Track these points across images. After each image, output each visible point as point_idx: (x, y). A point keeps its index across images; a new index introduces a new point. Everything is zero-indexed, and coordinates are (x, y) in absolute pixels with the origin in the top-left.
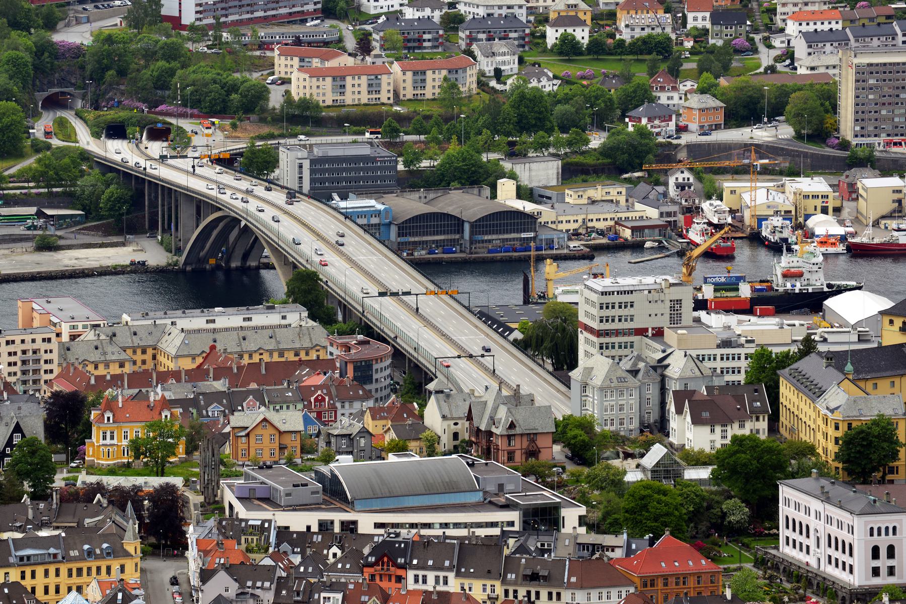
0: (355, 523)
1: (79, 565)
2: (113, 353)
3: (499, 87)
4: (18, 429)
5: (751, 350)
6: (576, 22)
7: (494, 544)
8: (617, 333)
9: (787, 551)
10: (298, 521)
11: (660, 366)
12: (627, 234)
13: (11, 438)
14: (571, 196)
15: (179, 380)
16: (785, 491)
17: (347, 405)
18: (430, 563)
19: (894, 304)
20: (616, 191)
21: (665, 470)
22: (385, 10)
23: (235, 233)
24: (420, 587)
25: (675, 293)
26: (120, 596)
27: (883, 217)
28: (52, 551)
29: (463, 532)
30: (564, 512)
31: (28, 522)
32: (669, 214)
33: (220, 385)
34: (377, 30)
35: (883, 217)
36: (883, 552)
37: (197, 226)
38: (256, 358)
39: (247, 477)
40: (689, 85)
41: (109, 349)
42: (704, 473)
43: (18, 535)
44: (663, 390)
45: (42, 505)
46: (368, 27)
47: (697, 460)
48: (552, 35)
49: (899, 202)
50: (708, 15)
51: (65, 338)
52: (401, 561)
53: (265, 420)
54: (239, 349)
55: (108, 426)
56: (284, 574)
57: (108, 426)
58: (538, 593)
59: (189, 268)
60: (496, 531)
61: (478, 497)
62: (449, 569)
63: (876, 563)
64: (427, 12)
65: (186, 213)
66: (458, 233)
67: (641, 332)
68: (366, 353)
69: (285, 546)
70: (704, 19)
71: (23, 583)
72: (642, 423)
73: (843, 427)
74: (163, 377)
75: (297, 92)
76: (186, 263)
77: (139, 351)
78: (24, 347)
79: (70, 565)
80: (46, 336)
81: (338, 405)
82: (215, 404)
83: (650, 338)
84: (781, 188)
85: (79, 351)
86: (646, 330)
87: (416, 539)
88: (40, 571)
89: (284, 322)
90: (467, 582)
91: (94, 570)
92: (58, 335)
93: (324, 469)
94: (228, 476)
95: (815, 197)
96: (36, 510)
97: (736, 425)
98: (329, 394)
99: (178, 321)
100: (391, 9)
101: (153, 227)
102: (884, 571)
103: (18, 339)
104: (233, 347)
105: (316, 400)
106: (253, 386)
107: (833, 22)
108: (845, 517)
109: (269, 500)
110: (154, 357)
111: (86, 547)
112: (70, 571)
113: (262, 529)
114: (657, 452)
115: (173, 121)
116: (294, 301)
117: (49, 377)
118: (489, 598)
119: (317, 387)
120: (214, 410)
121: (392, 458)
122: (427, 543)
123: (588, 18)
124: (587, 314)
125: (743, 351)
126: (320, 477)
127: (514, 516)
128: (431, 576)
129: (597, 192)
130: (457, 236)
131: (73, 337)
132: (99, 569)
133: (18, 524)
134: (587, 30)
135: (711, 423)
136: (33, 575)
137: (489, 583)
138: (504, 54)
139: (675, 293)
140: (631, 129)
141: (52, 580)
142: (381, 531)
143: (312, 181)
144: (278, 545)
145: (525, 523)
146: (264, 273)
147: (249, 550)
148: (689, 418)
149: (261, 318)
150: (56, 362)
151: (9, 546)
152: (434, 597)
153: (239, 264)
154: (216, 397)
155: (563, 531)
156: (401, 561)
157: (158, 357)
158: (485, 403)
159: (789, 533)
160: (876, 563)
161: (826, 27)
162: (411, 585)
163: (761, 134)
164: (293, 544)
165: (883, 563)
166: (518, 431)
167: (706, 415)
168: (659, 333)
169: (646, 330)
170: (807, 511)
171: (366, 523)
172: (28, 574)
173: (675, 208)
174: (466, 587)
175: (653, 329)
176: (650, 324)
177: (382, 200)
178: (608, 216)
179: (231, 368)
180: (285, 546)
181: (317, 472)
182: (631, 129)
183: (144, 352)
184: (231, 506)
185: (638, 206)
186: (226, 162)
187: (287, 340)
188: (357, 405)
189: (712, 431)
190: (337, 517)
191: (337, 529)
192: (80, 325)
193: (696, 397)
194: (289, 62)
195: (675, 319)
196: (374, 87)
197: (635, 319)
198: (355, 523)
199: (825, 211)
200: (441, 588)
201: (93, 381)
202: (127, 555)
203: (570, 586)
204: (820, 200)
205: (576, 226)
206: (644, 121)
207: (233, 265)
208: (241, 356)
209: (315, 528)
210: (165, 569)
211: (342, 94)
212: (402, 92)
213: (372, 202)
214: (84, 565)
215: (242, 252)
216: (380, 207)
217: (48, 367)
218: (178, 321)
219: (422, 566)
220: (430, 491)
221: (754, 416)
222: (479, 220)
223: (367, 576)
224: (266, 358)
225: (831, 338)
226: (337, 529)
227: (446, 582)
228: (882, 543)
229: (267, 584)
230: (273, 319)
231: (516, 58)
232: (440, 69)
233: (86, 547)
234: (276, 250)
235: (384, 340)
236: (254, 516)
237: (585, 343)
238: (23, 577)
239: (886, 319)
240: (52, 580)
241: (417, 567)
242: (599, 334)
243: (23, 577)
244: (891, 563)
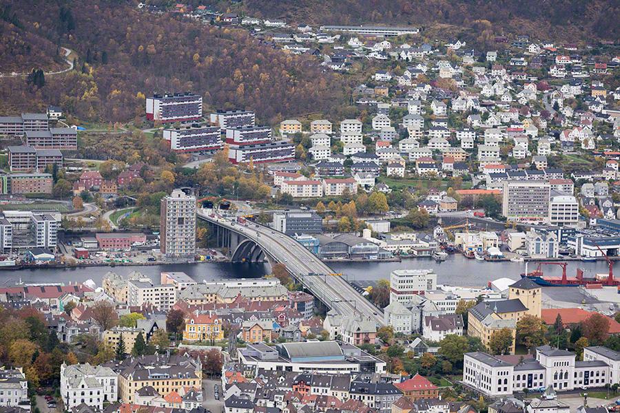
0: (291, 367)
1: (177, 381)
2: (199, 295)
3: (367, 191)
4: (155, 325)
5: (458, 300)
6: (399, 166)
7: (347, 377)
8: (406, 293)
9: (466, 381)
10: (267, 366)
11: (421, 306)
12: (415, 253)
13: (152, 328)
14: (394, 237)
15: (225, 308)
16: (466, 358)
17: (293, 319)
18: (320, 384)
19: (515, 282)
20: (412, 236)
21: (421, 348)
22: (321, 158)
23: (254, 247)
24: (316, 393)
25: (430, 277)
26: (192, 393)
27: (518, 249)
28: (166, 374)
29: (335, 372)
30: (377, 365)
31: (157, 362)
32: (432, 245)
33: (241, 310)
34: (317, 166)
35: (518, 249)
36: (503, 382)
37: (239, 243)
38: (257, 300)
39: (248, 347)
40: (444, 193)
41: (198, 294)
42: (435, 350)
44: (421, 316)
45: (163, 356)
46: (313, 165)
47: (434, 345)
48: (389, 171)
49: (524, 243)
50: (452, 164)
51: (180, 289)
52: (308, 383)
53: (257, 324)
54: (250, 296)
55: (192, 325)
57: (192, 325)
58: (364, 397)
60: (349, 372)
61: (342, 358)
62: (329, 386)
63: (500, 386)
64: (338, 160)
65: (234, 239)
67: (415, 292)
68: (303, 298)
69: (262, 376)
70: (451, 166)
73: (491, 332)
74: (218, 306)
75: (282, 191)
76: (233, 260)
77: (209, 295)
78: (162, 292)
79: (173, 381)
80: (171, 288)
81: (289, 319)
85: (185, 294)
87: (315, 374)
88: (161, 382)
89: (270, 285)
91: (183, 383)
93: (280, 345)
94: (241, 347)
96: (160, 357)
97: (450, 331)
98: (286, 315)
99: (226, 283)
101: (220, 246)
102: (502, 389)
103: (160, 289)
104: (248, 295)
106: (255, 311)
108: (488, 367)
109: (258, 358)
110: (216, 298)
111: (180, 373)
112: (173, 383)
113: (253, 368)
114: (418, 341)
115: (231, 201)
116: (276, 276)
117: (172, 304)
118: (344, 398)
119: (281, 312)
120: (238, 320)
121: (308, 341)
122: (319, 376)
123: (404, 164)
124: (394, 285)
125: (455, 301)
126: (278, 348)
127: (357, 366)
128: (321, 389)
129: (404, 236)
131: (183, 289)
132: (185, 382)
134: (403, 169)
135: (440, 330)
137: (344, 392)
139: (430, 277)
140: (419, 210)
141: (166, 386)
142: (302, 371)
143: (287, 228)
144: (258, 375)
145: (361, 369)
146: (265, 264)
147: (247, 377)
149: (261, 283)
150: (175, 298)
152: (321, 397)
153: (255, 261)
154: (239, 315)
155: (376, 372)
156: (308, 383)
159: (467, 374)
160: (500, 386)
161: (499, 172)
162: (312, 393)
164: (265, 375)
165: (503, 386)
166: (361, 331)
167: (438, 326)
168: (422, 293)
170: (475, 365)
171: (296, 368)
173: (436, 243)
176: (419, 289)
178: (408, 245)
180: (262, 376)
181: (277, 347)
182: (419, 210)
183: (211, 296)
184: (241, 359)
185: (420, 242)
187: (270, 292)
188: (297, 320)
190: (284, 365)
191: (284, 369)
192: (186, 284)
194: (280, 178)
195: (429, 287)
196: (314, 191)
198: (291, 367)
199: (495, 245)
200: (324, 394)
201: (189, 307)
202: (196, 377)
203: (376, 393)
205: (395, 249)
206: (425, 207)
208: (251, 299)
209: (275, 369)
210: (212, 383)
212: (326, 192)
213: (311, 237)
214: (179, 381)
216: (314, 239)
217: (172, 300)
218: (226, 283)
219: (317, 385)
220: (324, 355)
223: (294, 388)
224: (261, 300)
225: (491, 297)
226: (284, 369)
227: (326, 392)
228: (503, 378)
229: (253, 391)
230: (266, 283)
231: (374, 179)
232: (342, 183)
233: (180, 373)
234: (269, 256)
236: (250, 363)
237: (393, 297)
238: (154, 385)
239: (511, 289)
240: (166, 386)
241: (315, 386)
243: (154, 385)
244: (505, 386)
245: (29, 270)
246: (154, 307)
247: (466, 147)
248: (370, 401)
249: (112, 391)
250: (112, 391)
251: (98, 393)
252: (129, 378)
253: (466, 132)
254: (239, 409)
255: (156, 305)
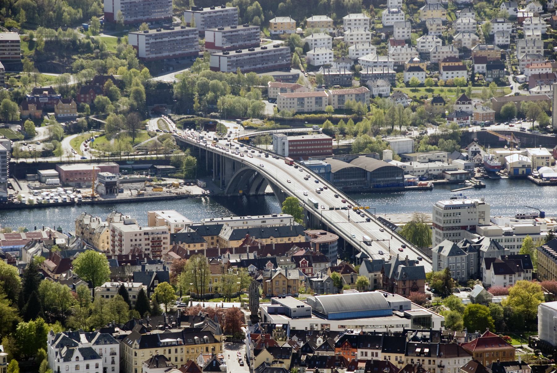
22: (322, 64)
26: (214, 362)
43: (162, 332)
50: (485, 65)
56: (295, 351)
59: (229, 195)
66: (364, 177)
67: (464, 228)
70: (483, 68)
71: (165, 355)
72: (468, 273)
76: (227, 193)
82: (252, 265)
83: (469, 231)
84: (526, 154)
86: (467, 226)
90: (387, 355)
92: (169, 230)
95: (543, 158)
100: (325, 63)
105: (302, 263)
107: (548, 69)
119: (302, 257)
130: (364, 179)
133: (161, 326)
136: (170, 352)
138: (383, 86)
143: (290, 150)
148: (493, 272)
151: (60, 341)
153: (254, 193)
157: (220, 241)
158: (390, 265)
163: (517, 126)
169: (467, 226)
172: (167, 351)
174: (387, 358)
175: (470, 226)
176: (469, 224)
177: (326, 161)
179: (258, 247)
186: (244, 142)
189: (505, 278)
193: (496, 262)
197: (461, 221)
199: (548, 165)
200: (375, 358)
204: (545, 159)
207: (251, 193)
211: (303, 107)
215: (256, 187)
221: (525, 270)
222: (375, 170)
227: (377, 356)
235: (334, 232)
238: (165, 353)
242: (442, 229)
245: (36, 210)
246: (145, 254)
247: (501, 43)
248: (432, 366)
249: (113, 362)
250: (113, 362)
251: (97, 367)
252: (134, 346)
253: (501, 24)
254: (388, 220)
255: (147, 252)
